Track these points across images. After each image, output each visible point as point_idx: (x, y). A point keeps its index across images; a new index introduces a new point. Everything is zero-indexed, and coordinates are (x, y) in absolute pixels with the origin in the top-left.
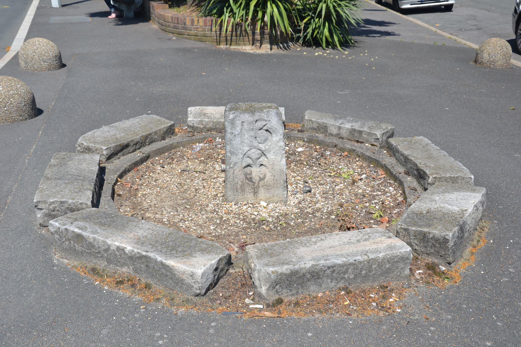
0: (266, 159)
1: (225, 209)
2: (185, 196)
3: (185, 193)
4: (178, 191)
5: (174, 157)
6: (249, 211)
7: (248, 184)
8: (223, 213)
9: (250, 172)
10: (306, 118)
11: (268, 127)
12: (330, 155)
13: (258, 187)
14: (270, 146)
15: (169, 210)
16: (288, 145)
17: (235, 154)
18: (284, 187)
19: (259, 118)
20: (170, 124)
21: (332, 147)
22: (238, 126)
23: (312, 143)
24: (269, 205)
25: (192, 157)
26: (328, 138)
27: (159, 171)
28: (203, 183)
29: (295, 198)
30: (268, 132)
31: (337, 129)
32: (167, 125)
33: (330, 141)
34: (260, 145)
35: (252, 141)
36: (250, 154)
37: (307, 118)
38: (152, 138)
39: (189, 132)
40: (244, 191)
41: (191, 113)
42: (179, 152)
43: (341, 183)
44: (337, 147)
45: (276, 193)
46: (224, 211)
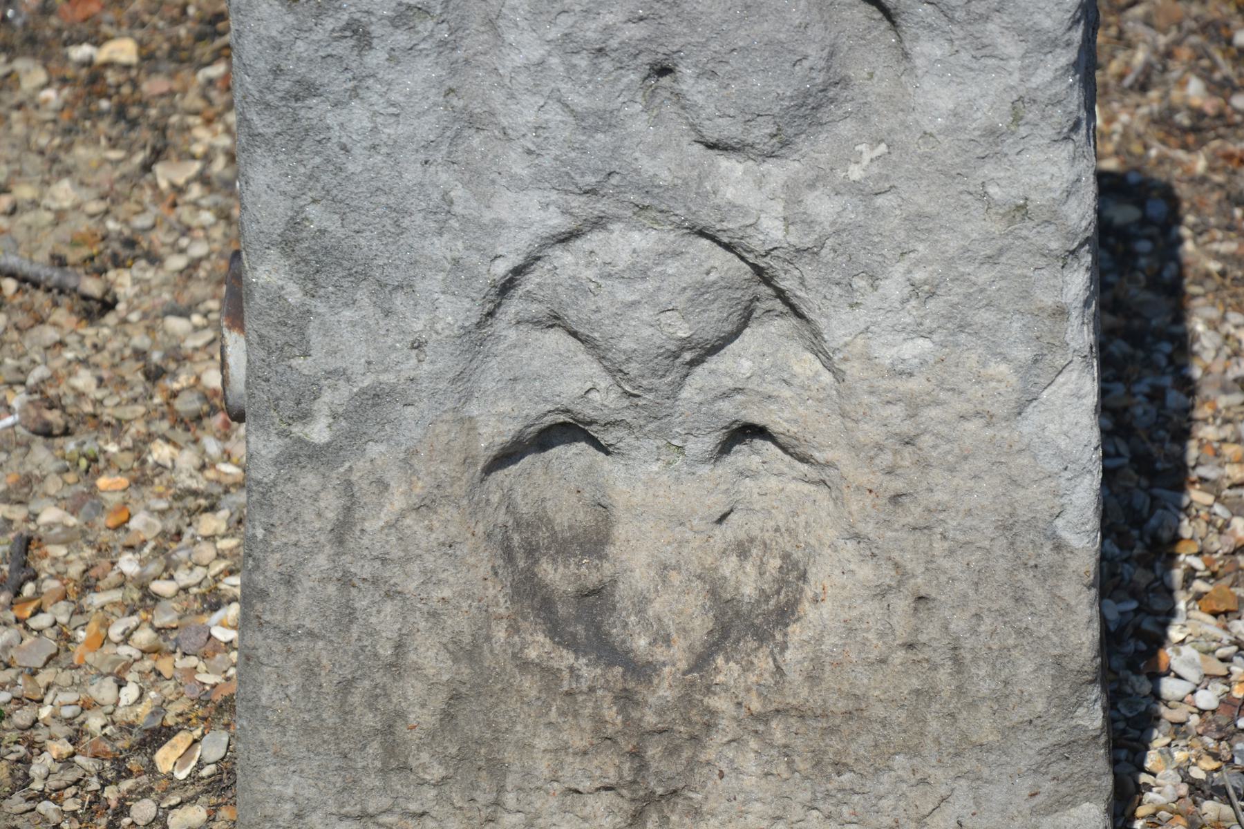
0: (806, 365)
7: (549, 674)
9: (584, 518)
14: (865, 193)
17: (359, 275)
18: (1069, 748)
34: (727, 164)
35: (604, 121)
36: (579, 288)
40: (496, 769)
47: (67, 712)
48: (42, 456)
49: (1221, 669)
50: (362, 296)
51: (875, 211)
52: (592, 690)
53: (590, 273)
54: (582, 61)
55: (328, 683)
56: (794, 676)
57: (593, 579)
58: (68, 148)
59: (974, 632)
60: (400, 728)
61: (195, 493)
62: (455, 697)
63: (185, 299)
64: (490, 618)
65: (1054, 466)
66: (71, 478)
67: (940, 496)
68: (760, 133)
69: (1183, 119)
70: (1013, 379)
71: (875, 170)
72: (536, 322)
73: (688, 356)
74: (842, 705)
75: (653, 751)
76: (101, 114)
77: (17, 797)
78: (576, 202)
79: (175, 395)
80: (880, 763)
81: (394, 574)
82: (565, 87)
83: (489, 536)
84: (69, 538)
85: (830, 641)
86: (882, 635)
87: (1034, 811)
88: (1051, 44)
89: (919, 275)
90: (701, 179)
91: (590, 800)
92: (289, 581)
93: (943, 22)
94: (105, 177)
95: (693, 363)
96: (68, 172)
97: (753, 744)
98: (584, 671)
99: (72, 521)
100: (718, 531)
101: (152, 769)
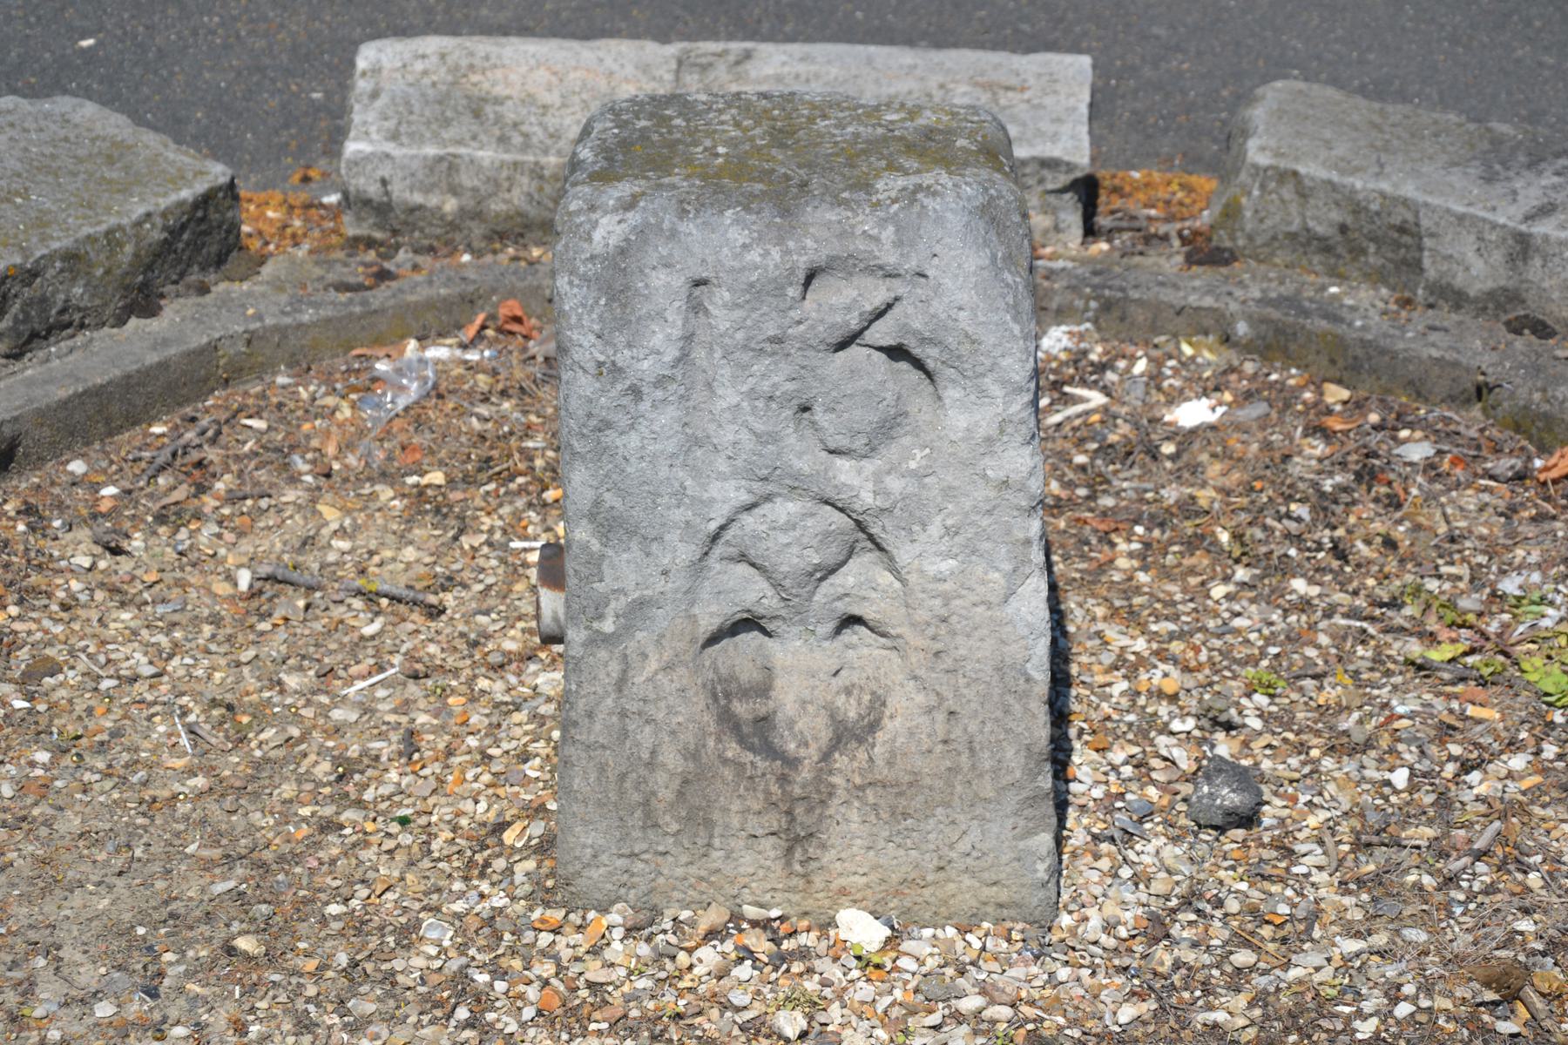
0: (886, 578)
1: (546, 969)
2: (252, 829)
3: (256, 795)
4: (200, 782)
5: (212, 454)
6: (738, 998)
7: (739, 766)
8: (528, 1013)
9: (757, 676)
10: (1257, 152)
11: (905, 329)
12: (1430, 467)
13: (820, 794)
14: (918, 476)
15: (89, 975)
16: (1101, 368)
17: (632, 533)
18: (1032, 801)
19: (834, 248)
20: (201, 187)
21: (1451, 399)
22: (660, 315)
23: (1289, 359)
24: (907, 946)
25: (352, 460)
26: (1420, 318)
27: (75, 585)
28: (405, 707)
29: (1126, 872)
30: (904, 365)
31: (1498, 257)
32: (173, 198)
33: (1436, 348)
34: (840, 462)
35: (773, 438)
36: (757, 537)
37: (1264, 160)
38: (44, 301)
39: (355, 243)
40: (709, 824)
41: (375, 95)
42: (258, 414)
43: (1513, 746)
44: (1491, 399)
45: (964, 846)
46: (532, 993)
47: (448, 818)
48: (413, 689)
49: (1103, 778)
50: (634, 545)
51: (924, 486)
52: (764, 775)
53: (764, 527)
54: (760, 404)
55: (612, 775)
56: (880, 762)
57: (763, 711)
58: (410, 530)
59: (981, 732)
60: (653, 801)
61: (506, 703)
62: (686, 782)
63: (485, 606)
64: (705, 734)
65: (1026, 632)
66: (432, 699)
67: (962, 652)
68: (859, 443)
69: (1050, 501)
70: (1002, 581)
71: (924, 462)
72: (731, 559)
73: (818, 575)
74: (907, 778)
75: (799, 810)
76: (427, 512)
77: (426, 860)
78: (756, 486)
79: (487, 654)
80: (928, 812)
81: (650, 709)
82: (750, 419)
83: (704, 686)
84: (435, 730)
85: (901, 740)
86: (929, 736)
87: (1014, 838)
88: (1020, 390)
89: (949, 522)
90: (826, 470)
91: (763, 841)
92: (590, 715)
93: (960, 378)
94: (432, 544)
95: (822, 579)
96: (411, 543)
97: (856, 804)
98: (759, 764)
99: (435, 722)
100: (834, 681)
101: (501, 843)
